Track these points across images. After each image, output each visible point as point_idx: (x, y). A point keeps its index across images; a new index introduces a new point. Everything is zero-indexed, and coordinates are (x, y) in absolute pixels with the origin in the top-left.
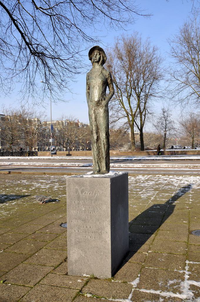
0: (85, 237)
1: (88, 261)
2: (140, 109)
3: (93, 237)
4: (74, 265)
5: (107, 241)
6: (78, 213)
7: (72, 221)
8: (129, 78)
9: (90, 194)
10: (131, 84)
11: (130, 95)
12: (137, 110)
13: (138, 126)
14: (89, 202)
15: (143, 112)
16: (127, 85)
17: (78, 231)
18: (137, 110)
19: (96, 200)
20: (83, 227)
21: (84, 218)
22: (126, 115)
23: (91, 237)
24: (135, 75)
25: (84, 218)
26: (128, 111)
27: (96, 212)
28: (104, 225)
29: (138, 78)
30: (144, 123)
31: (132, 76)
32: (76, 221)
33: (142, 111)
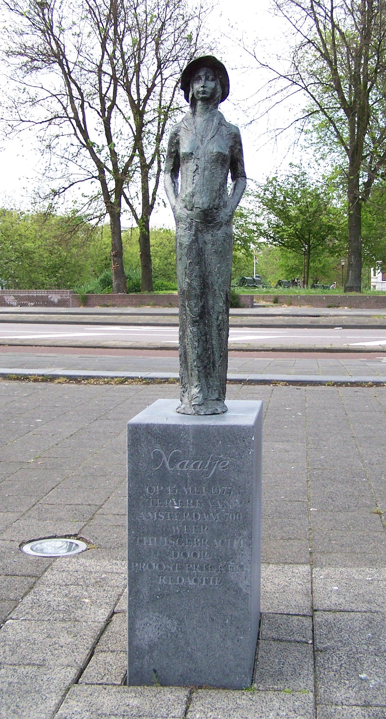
0: (180, 580)
1: (187, 643)
2: (142, 155)
3: (202, 579)
4: (147, 657)
5: (241, 589)
6: (161, 518)
7: (141, 541)
8: (110, 48)
9: (195, 466)
10: (114, 69)
11: (111, 108)
12: (132, 158)
13: (133, 211)
14: (193, 489)
15: (152, 162)
16: (100, 72)
17: (160, 566)
18: (132, 158)
19: (213, 481)
20: (176, 556)
21: (176, 531)
22: (97, 174)
23: (196, 581)
24: (128, 40)
25: (176, 531)
26: (101, 157)
27: (211, 514)
28: (235, 546)
29: (139, 49)
30: (154, 199)
31: (118, 40)
32: (152, 540)
33: (148, 162)
